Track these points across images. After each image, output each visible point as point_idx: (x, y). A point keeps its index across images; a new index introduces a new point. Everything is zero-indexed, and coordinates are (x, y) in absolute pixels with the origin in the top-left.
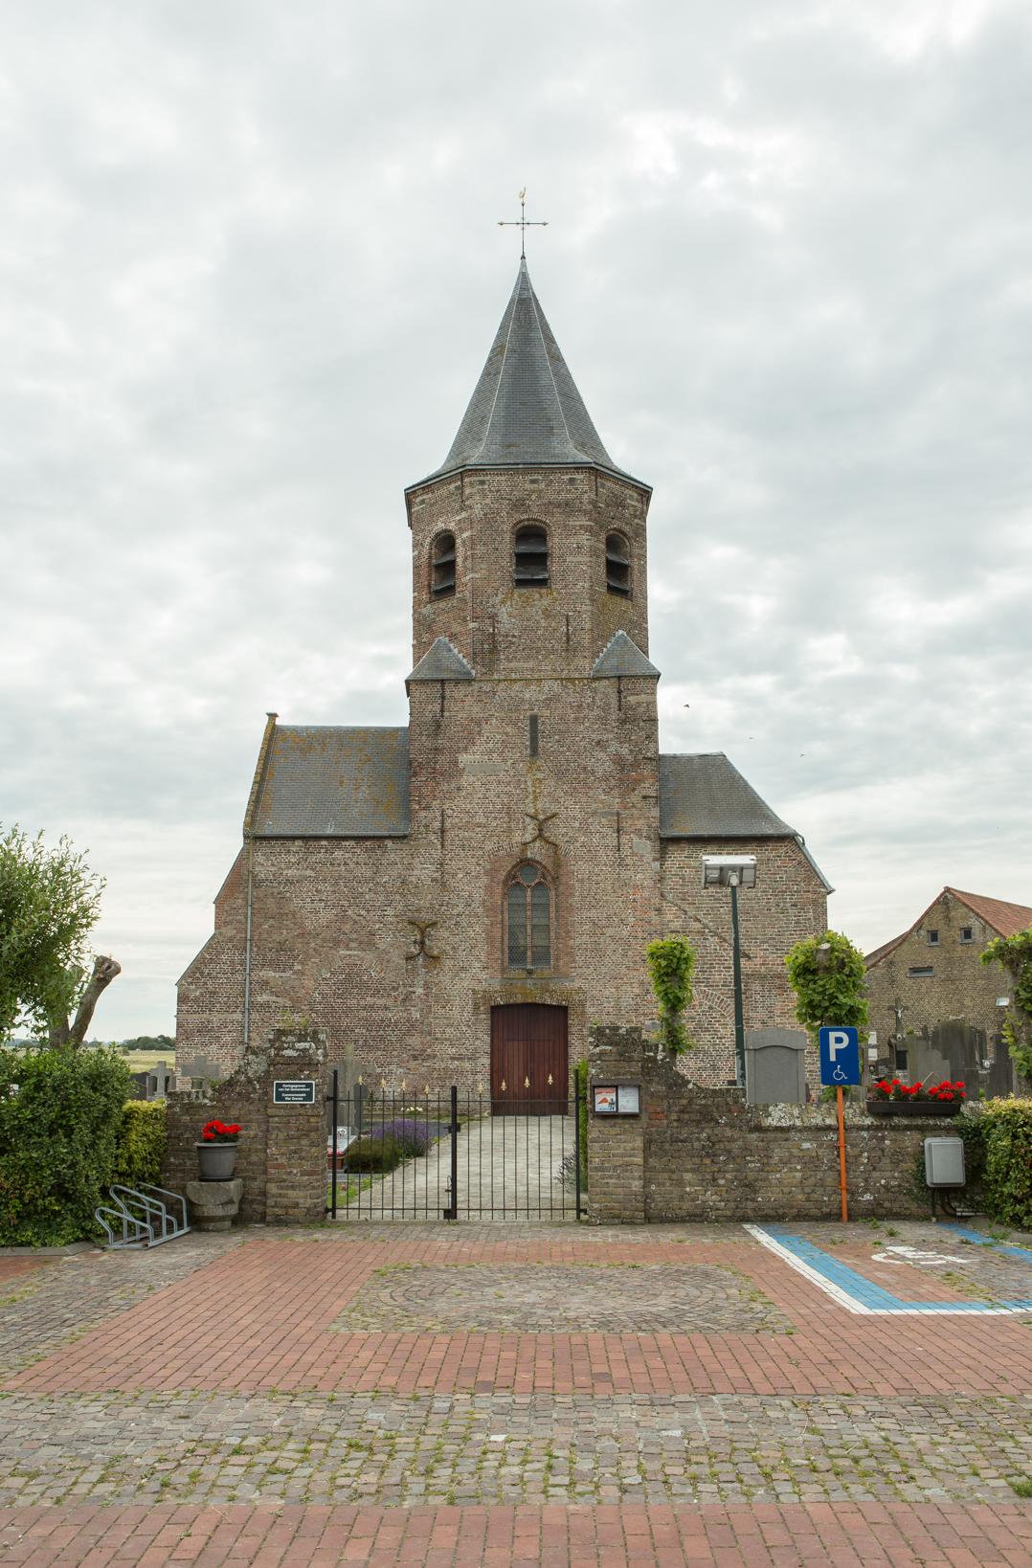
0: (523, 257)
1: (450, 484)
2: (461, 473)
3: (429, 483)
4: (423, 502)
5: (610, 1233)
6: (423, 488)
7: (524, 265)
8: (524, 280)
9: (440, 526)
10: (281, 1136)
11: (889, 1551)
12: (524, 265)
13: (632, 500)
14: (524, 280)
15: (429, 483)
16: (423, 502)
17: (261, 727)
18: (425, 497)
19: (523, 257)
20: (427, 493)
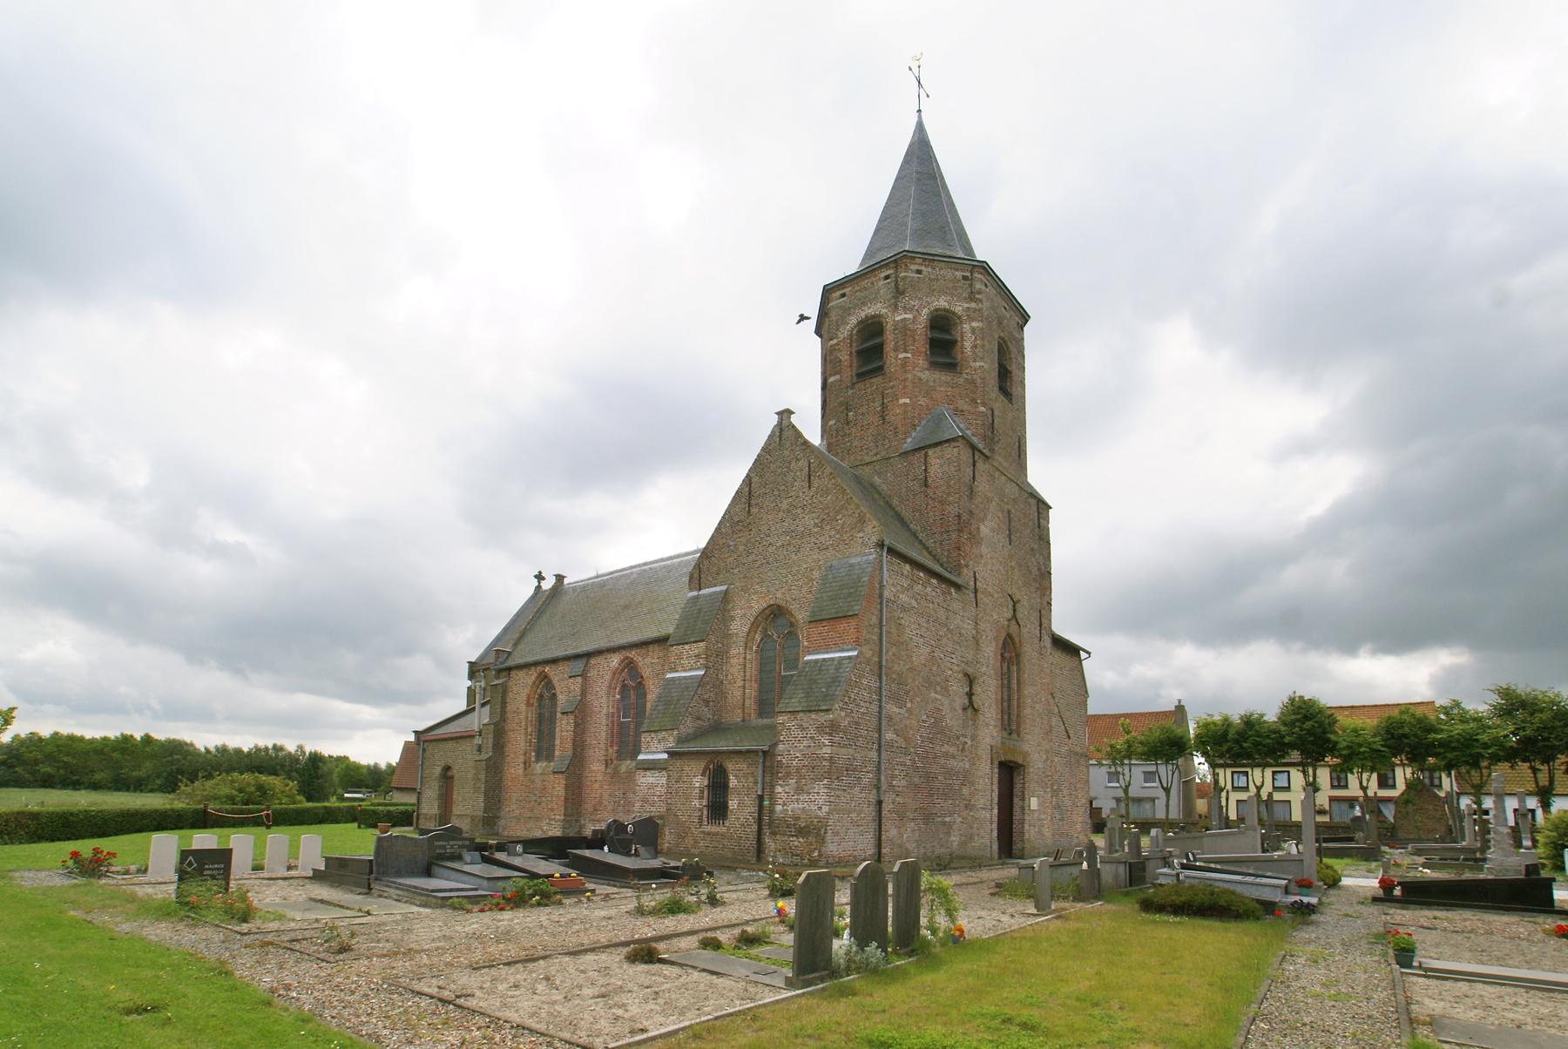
0: (919, 111)
1: (957, 270)
2: (973, 265)
3: (936, 258)
4: (919, 272)
5: (518, 834)
6: (925, 260)
7: (920, 117)
8: (920, 128)
9: (942, 303)
10: (935, 844)
11: (853, 622)
12: (920, 117)
13: (1013, 319)
14: (920, 128)
15: (936, 258)
16: (919, 272)
17: (1051, 505)
18: (923, 268)
19: (919, 111)
20: (926, 266)
